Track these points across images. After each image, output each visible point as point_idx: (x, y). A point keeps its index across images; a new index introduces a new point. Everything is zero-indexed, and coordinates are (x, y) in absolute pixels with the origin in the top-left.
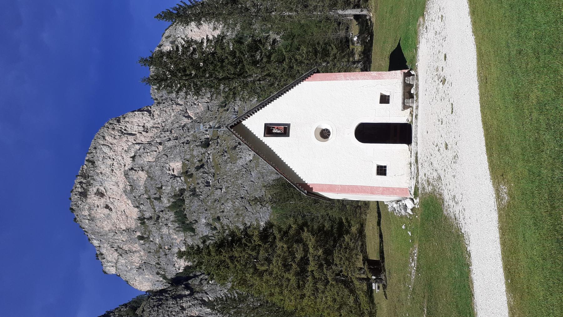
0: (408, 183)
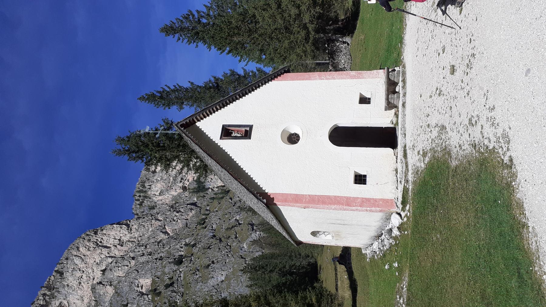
0: (393, 193)
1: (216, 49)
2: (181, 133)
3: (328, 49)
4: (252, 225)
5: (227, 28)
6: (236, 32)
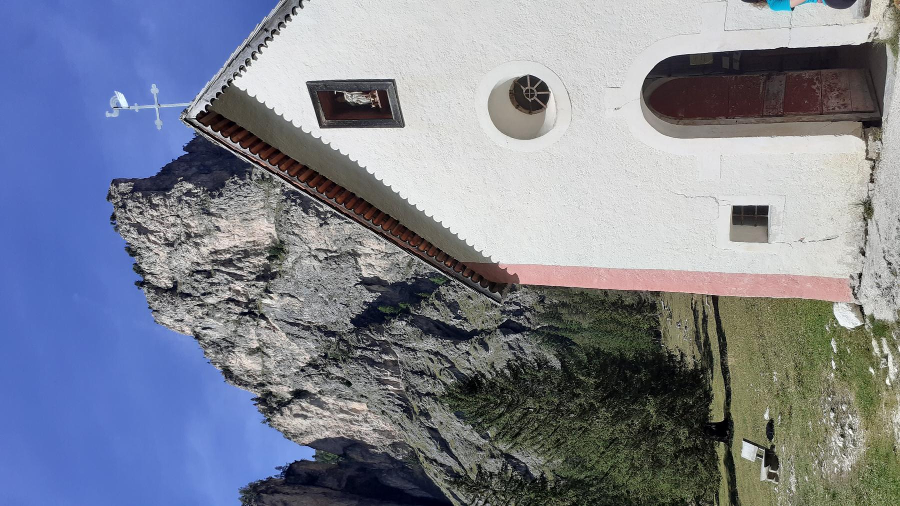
0: (849, 265)
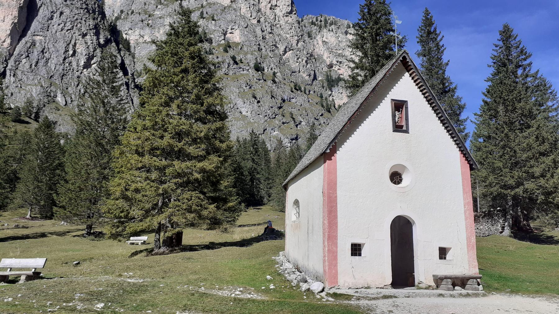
0: (344, 284)
1: (488, 88)
2: (397, 58)
3: (495, 211)
4: (296, 139)
5: (513, 98)
6: (508, 108)
